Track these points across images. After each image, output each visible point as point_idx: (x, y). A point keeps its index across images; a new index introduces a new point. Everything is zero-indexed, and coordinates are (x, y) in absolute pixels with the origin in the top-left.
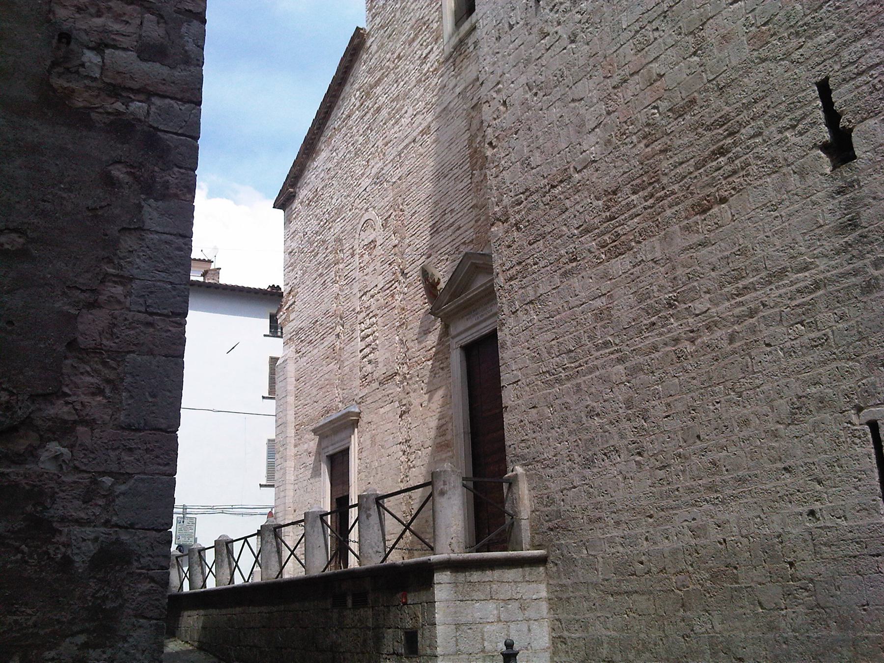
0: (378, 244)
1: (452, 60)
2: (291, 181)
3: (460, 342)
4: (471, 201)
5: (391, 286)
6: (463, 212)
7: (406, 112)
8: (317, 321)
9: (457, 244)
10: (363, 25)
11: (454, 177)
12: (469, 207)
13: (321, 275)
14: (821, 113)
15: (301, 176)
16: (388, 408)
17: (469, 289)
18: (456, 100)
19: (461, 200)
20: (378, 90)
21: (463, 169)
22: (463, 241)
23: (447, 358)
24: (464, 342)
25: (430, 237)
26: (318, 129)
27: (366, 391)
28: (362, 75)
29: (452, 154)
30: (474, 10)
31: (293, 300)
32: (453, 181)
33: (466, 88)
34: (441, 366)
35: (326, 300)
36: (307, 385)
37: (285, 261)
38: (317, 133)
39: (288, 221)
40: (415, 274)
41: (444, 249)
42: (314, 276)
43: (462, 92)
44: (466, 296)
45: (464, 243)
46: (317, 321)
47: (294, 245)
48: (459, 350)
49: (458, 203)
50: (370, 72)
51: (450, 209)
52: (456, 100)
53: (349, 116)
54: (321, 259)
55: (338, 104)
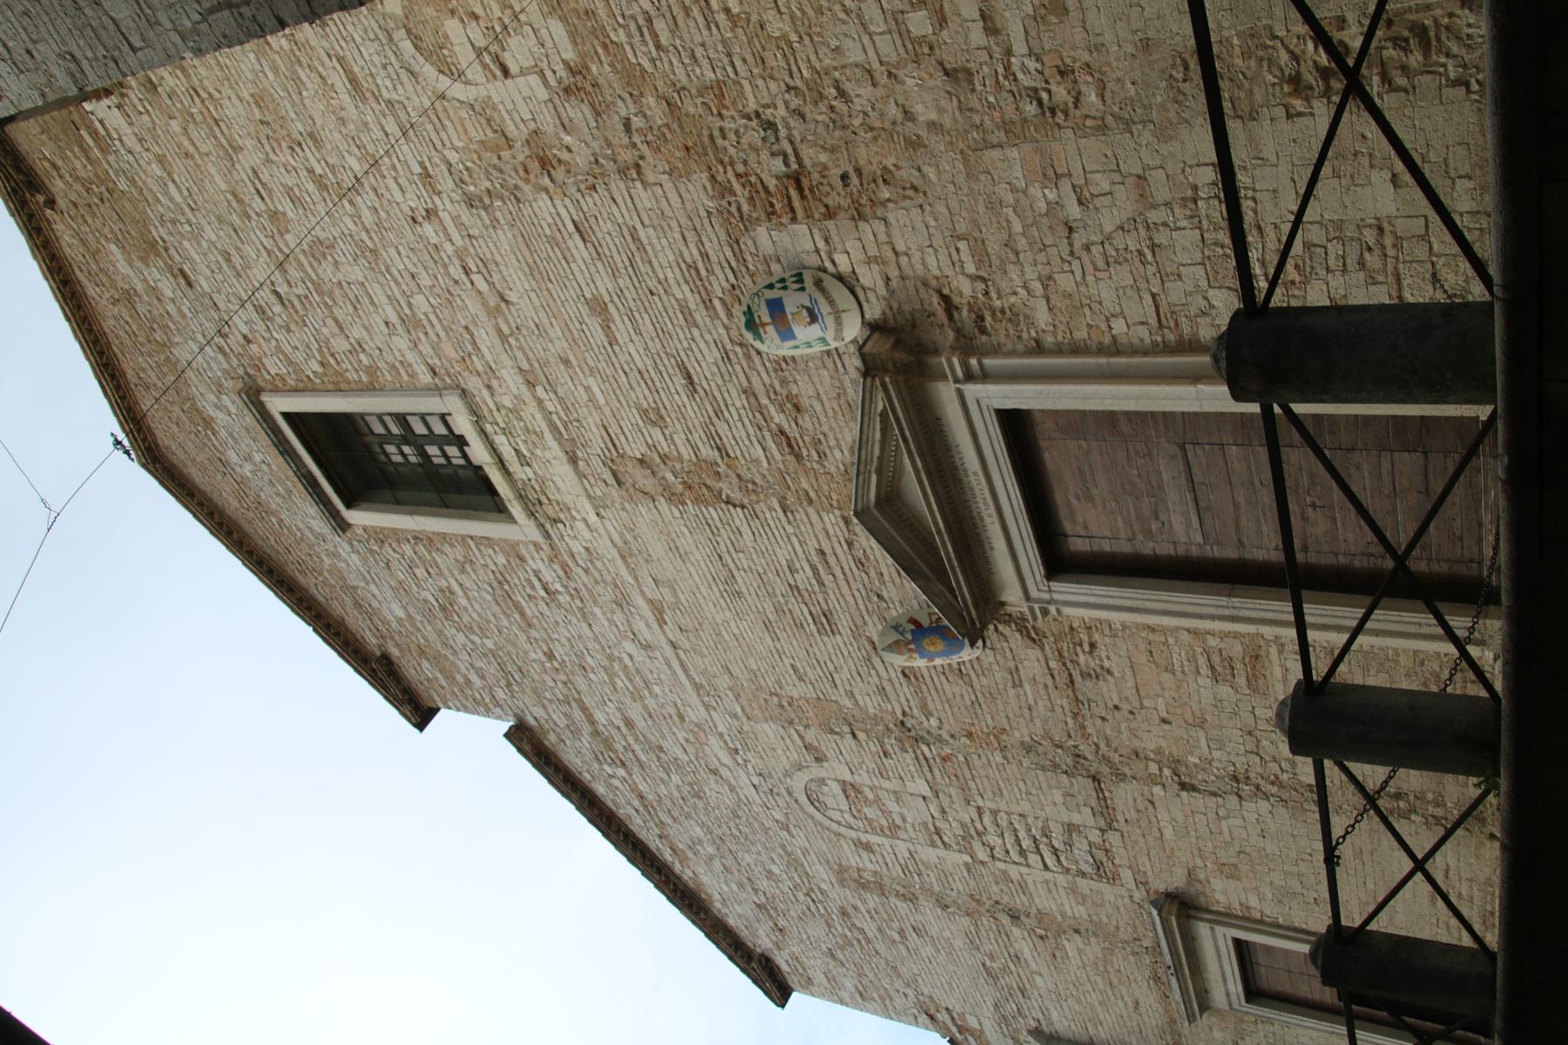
0: (848, 777)
1: (548, 526)
2: (742, 957)
3: (1038, 578)
4: (770, 509)
5: (926, 758)
6: (794, 539)
7: (631, 657)
8: (984, 965)
9: (851, 562)
10: (505, 726)
11: (732, 551)
12: (783, 519)
13: (901, 932)
14: (1261, 961)
15: (735, 934)
16: (1164, 817)
17: (930, 533)
18: (608, 524)
19: (772, 539)
20: (600, 717)
21: (720, 526)
22: (845, 547)
23: (1072, 628)
24: (1039, 570)
25: (838, 637)
26: (659, 872)
27: (1126, 875)
28: (576, 755)
29: (695, 551)
30: (462, 436)
31: (944, 1012)
32: (740, 555)
33: (589, 497)
34: (1087, 648)
35: (947, 934)
36: (1102, 1018)
37: (875, 1012)
38: (667, 877)
39: (808, 985)
40: (906, 690)
41: (860, 602)
42: (904, 952)
43: (596, 507)
44: (939, 532)
45: (850, 544)
46: (984, 965)
47: (849, 984)
48: (1055, 585)
49: (777, 550)
50: (576, 733)
51: (788, 573)
52: (608, 524)
53: (641, 797)
54: (874, 927)
55: (623, 817)
